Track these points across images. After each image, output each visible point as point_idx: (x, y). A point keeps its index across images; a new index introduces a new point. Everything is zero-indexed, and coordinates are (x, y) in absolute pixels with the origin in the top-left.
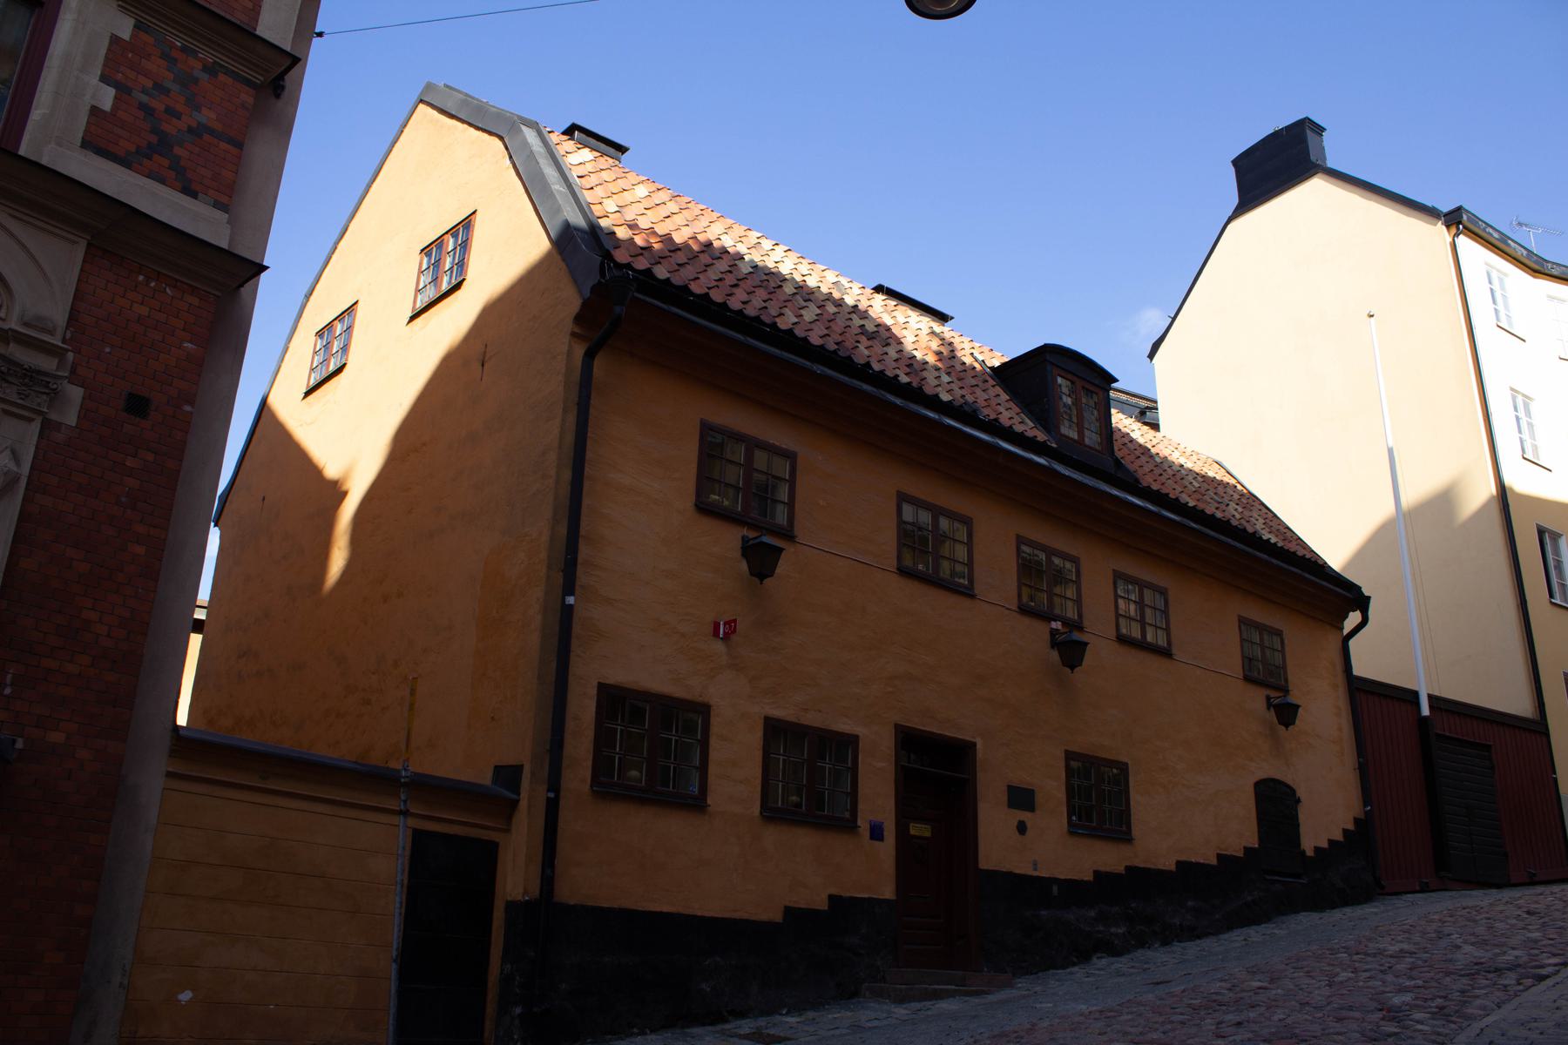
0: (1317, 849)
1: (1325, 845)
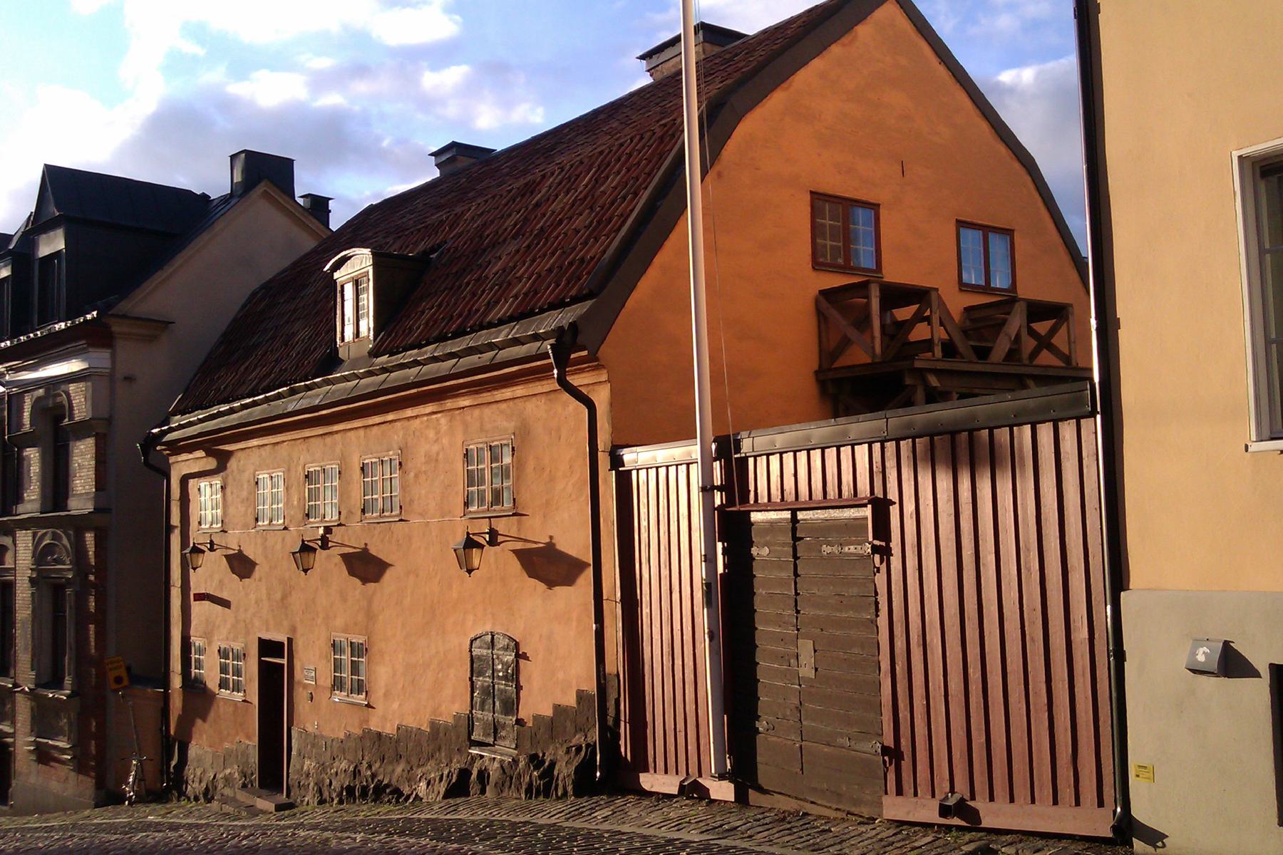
0: (537, 718)
1: (549, 712)
